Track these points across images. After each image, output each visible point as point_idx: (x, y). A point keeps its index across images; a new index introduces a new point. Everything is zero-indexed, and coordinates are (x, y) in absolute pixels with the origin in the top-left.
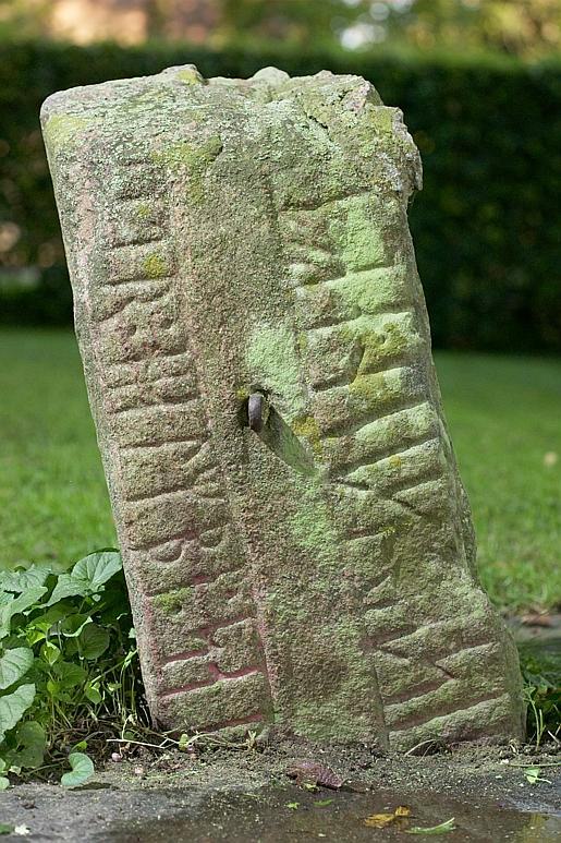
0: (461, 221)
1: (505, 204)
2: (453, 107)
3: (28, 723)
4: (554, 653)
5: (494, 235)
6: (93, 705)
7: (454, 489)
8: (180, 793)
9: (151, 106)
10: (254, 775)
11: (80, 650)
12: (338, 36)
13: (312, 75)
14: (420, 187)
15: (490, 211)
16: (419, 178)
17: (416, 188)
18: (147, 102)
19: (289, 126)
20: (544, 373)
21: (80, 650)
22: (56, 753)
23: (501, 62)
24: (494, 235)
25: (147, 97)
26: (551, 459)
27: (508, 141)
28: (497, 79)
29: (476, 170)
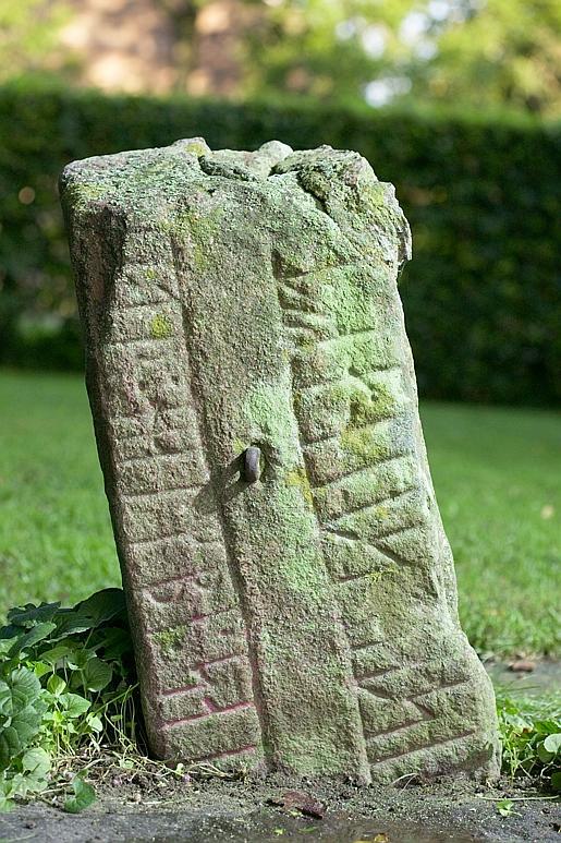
0: (478, 276)
1: (521, 260)
2: (472, 163)
3: (35, 749)
4: (533, 696)
5: (509, 290)
6: (95, 734)
7: (437, 538)
8: (173, 817)
9: (162, 176)
10: (243, 802)
11: (84, 683)
12: (364, 88)
13: (313, 148)
14: (410, 257)
15: (506, 266)
16: (409, 249)
17: (405, 258)
18: (157, 173)
19: (287, 198)
20: (544, 426)
21: (84, 683)
22: (60, 778)
23: (518, 118)
24: (509, 290)
25: (158, 167)
26: (548, 512)
27: (525, 197)
28: (516, 137)
29: (492, 225)
